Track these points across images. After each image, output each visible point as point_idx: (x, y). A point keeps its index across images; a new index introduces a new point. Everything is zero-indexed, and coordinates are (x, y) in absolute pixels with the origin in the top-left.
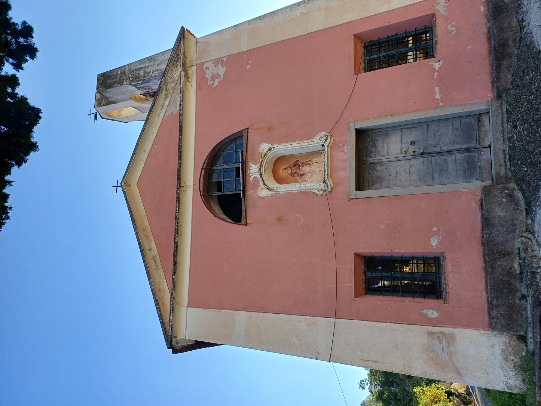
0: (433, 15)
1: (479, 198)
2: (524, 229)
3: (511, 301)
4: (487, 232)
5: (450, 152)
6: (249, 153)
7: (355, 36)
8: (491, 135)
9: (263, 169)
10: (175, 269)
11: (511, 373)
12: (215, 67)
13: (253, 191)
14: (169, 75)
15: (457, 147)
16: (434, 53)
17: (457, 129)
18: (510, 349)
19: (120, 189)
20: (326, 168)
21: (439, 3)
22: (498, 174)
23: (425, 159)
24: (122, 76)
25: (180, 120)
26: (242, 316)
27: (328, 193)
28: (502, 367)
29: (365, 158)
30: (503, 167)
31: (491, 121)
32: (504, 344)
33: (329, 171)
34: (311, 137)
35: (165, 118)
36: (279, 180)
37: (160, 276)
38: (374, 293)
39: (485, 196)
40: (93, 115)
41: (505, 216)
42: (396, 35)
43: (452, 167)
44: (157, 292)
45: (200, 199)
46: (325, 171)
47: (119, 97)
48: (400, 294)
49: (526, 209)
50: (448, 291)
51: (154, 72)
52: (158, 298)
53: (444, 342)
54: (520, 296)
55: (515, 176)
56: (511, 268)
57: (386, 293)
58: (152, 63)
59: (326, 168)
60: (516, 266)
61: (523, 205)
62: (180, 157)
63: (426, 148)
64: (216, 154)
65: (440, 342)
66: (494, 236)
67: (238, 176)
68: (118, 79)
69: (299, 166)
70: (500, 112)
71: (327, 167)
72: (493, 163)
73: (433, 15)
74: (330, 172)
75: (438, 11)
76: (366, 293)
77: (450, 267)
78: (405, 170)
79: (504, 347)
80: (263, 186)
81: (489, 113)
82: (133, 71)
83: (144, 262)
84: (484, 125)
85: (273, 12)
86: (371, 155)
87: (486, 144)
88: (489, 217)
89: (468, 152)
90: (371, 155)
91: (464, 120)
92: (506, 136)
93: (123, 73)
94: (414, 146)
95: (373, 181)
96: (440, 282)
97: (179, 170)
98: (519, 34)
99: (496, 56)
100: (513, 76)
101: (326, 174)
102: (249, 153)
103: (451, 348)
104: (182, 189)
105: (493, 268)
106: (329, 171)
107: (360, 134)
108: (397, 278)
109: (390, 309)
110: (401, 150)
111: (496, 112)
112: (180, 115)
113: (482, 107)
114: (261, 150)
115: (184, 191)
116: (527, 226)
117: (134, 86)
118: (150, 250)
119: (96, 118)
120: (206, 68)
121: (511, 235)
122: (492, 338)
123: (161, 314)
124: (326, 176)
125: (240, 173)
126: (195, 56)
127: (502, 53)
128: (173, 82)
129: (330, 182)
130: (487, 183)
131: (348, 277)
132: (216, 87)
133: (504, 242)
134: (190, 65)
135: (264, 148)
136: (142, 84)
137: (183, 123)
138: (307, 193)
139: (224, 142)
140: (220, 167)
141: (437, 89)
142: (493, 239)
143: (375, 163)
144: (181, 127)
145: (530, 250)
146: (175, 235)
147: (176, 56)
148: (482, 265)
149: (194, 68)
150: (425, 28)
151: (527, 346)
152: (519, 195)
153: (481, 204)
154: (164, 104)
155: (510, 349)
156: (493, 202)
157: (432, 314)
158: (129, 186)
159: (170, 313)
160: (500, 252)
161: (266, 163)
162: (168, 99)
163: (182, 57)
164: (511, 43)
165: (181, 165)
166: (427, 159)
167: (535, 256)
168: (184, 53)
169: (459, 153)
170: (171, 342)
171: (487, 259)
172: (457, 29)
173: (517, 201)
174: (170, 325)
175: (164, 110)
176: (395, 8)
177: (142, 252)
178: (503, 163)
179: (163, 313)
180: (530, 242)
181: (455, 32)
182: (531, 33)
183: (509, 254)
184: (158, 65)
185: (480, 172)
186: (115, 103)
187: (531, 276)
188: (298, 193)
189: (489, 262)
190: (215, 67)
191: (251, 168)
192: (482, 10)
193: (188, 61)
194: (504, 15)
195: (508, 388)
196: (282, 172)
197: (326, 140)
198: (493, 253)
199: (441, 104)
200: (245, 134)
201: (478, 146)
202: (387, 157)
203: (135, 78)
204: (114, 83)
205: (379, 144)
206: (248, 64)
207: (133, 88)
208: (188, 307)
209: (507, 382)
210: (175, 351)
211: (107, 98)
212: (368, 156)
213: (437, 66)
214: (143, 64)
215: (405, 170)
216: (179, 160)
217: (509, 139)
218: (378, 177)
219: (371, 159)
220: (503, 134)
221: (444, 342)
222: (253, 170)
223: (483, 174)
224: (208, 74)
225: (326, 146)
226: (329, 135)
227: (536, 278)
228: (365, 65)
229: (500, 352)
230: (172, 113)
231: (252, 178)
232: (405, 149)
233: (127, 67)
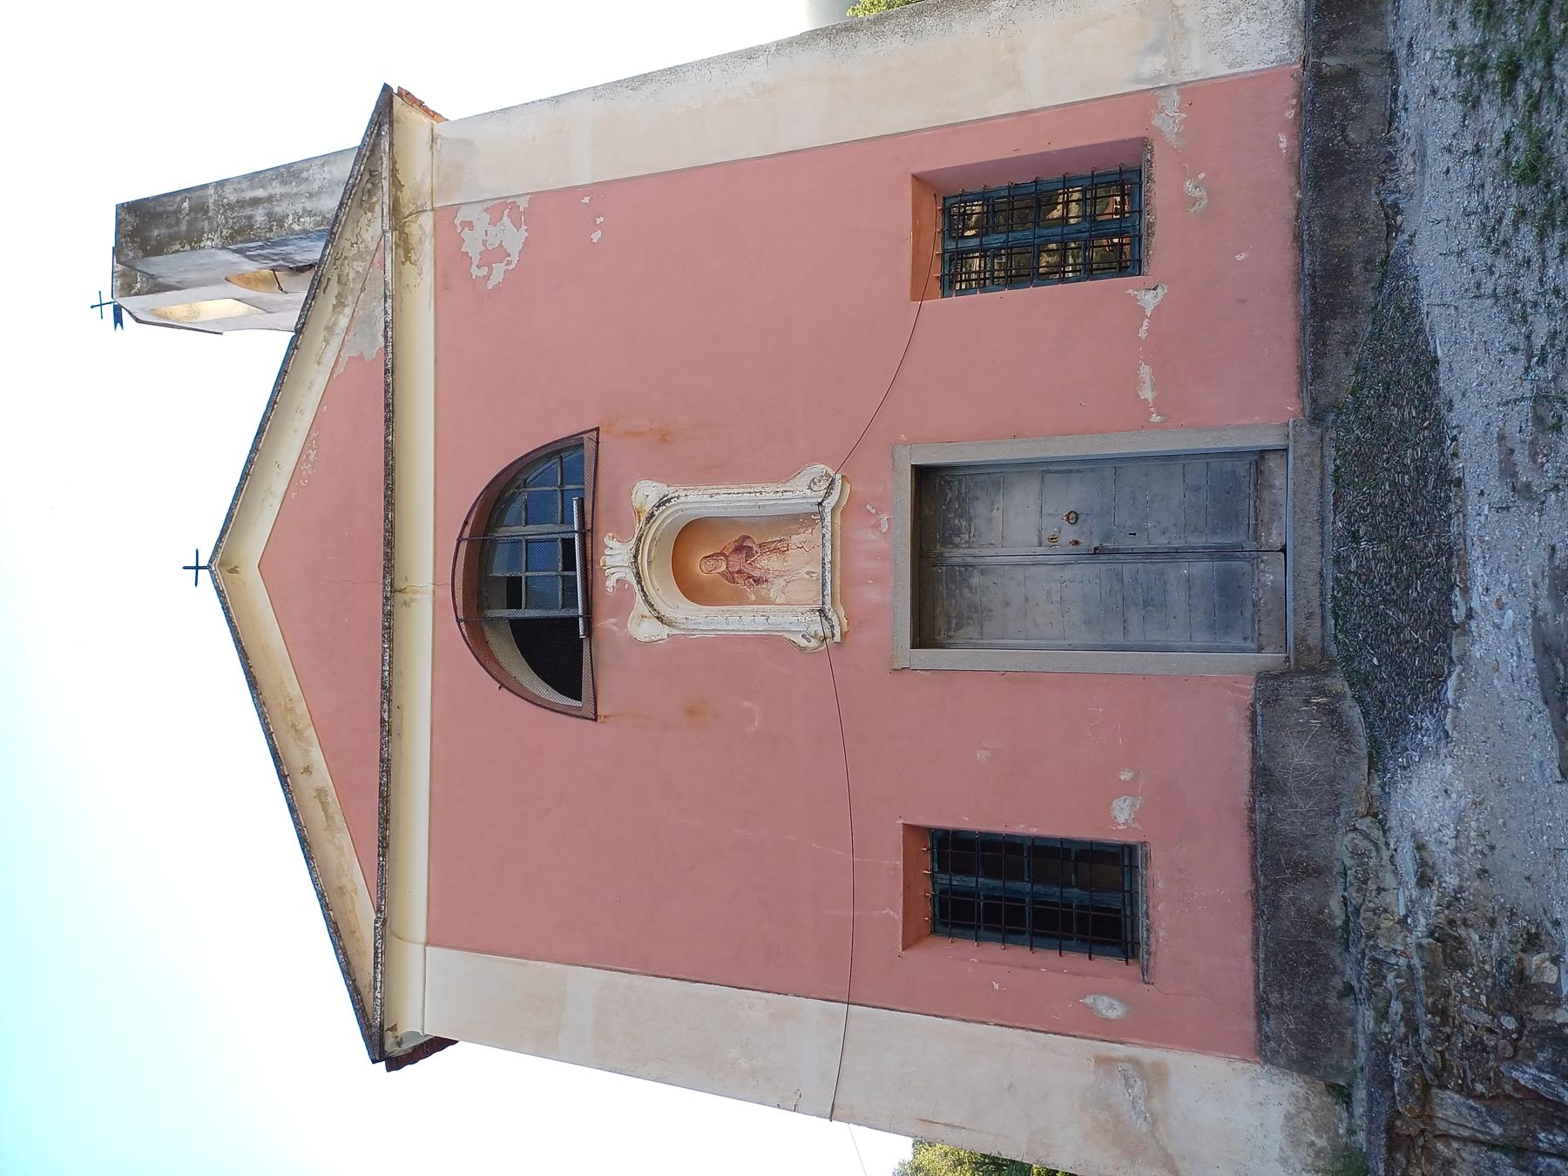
0: (1144, 143)
1: (1249, 699)
2: (1362, 808)
3: (1316, 999)
5: (1173, 554)
6: (601, 504)
7: (917, 178)
8: (1290, 515)
12: (493, 223)
13: (613, 620)
14: (348, 234)
15: (1195, 540)
17: (1197, 489)
18: (1308, 1115)
19: (204, 575)
22: (1301, 639)
23: (1104, 567)
24: (196, 220)
25: (387, 385)
26: (586, 982)
27: (834, 647)
28: (1284, 1161)
30: (1317, 622)
32: (1292, 1100)
33: (838, 582)
34: (784, 474)
35: (340, 370)
36: (692, 590)
37: (340, 849)
39: (1263, 706)
40: (109, 310)
41: (1314, 768)
42: (1036, 182)
43: (1177, 596)
44: (332, 899)
46: (824, 585)
47: (192, 276)
49: (1370, 755)
50: (1153, 949)
52: (339, 919)
54: (1340, 986)
55: (1349, 659)
56: (1321, 912)
58: (293, 188)
60: (1335, 904)
61: (1362, 745)
62: (390, 502)
63: (1107, 536)
64: (503, 492)
65: (1128, 1086)
66: (1280, 820)
67: (569, 564)
69: (749, 552)
70: (1317, 460)
72: (1290, 605)
73: (1144, 143)
74: (840, 583)
75: (1159, 132)
76: (934, 932)
77: (1160, 885)
78: (1049, 594)
79: (1292, 1110)
80: (645, 610)
82: (231, 207)
83: (292, 809)
84: (1272, 486)
86: (957, 540)
87: (1275, 540)
88: (1271, 765)
89: (1224, 558)
90: (957, 540)
92: (1331, 549)
93: (200, 209)
96: (1134, 916)
97: (389, 543)
98: (1383, 246)
99: (1314, 302)
100: (1357, 370)
101: (828, 591)
102: (602, 504)
103: (1156, 1103)
104: (400, 597)
105: (1275, 905)
106: (838, 582)
107: (924, 476)
108: (1019, 896)
110: (1040, 536)
111: (1307, 460)
112: (386, 371)
113: (1271, 440)
115: (405, 603)
116: (1370, 799)
117: (235, 251)
118: (307, 770)
119: (118, 319)
120: (463, 224)
121: (1326, 822)
122: (1262, 1082)
123: (348, 963)
124: (828, 599)
125: (576, 555)
127: (1332, 296)
128: (359, 256)
129: (838, 616)
130: (1271, 658)
131: (885, 886)
132: (497, 287)
133: (1307, 837)
134: (412, 207)
135: (645, 495)
136: (261, 247)
138: (773, 643)
141: (1145, 371)
142: (1278, 827)
143: (966, 566)
144: (390, 407)
145: (1372, 886)
146: (382, 738)
147: (366, 177)
148: (1246, 885)
149: (426, 221)
151: (1351, 1115)
152: (1356, 713)
153: (1253, 720)
154: (335, 324)
156: (1284, 727)
157: (1110, 1008)
158: (234, 570)
159: (376, 963)
160: (1296, 865)
162: (348, 311)
163: (386, 184)
164: (1357, 268)
166: (1112, 567)
167: (1385, 911)
168: (394, 171)
169: (1199, 559)
170: (382, 1045)
172: (1210, 195)
173: (1348, 730)
174: (375, 998)
175: (335, 342)
176: (1036, 107)
177: (283, 778)
178: (1318, 611)
179: (355, 961)
180: (1374, 854)
181: (1204, 203)
182: (1416, 279)
183: (1318, 872)
184: (311, 196)
187: (1372, 971)
188: (744, 637)
189: (1265, 888)
190: (493, 223)
191: (608, 552)
193: (406, 195)
194: (1345, 180)
196: (703, 568)
197: (828, 493)
198: (1279, 865)
199: (1155, 418)
200: (589, 446)
202: (1001, 551)
203: (240, 231)
204: (173, 238)
205: (979, 509)
206: (596, 227)
207: (236, 258)
208: (427, 944)
210: (394, 1064)
211: (151, 276)
212: (947, 541)
213: (1149, 300)
214: (263, 187)
215: (1049, 594)
216: (386, 509)
217: (1337, 560)
219: (957, 552)
220: (1322, 525)
222: (615, 558)
223: (1263, 625)
224: (473, 247)
225: (828, 510)
226: (838, 476)
227: (1385, 978)
229: (1281, 1121)
230: (361, 356)
231: (611, 583)
232: (1050, 533)
233: (211, 191)
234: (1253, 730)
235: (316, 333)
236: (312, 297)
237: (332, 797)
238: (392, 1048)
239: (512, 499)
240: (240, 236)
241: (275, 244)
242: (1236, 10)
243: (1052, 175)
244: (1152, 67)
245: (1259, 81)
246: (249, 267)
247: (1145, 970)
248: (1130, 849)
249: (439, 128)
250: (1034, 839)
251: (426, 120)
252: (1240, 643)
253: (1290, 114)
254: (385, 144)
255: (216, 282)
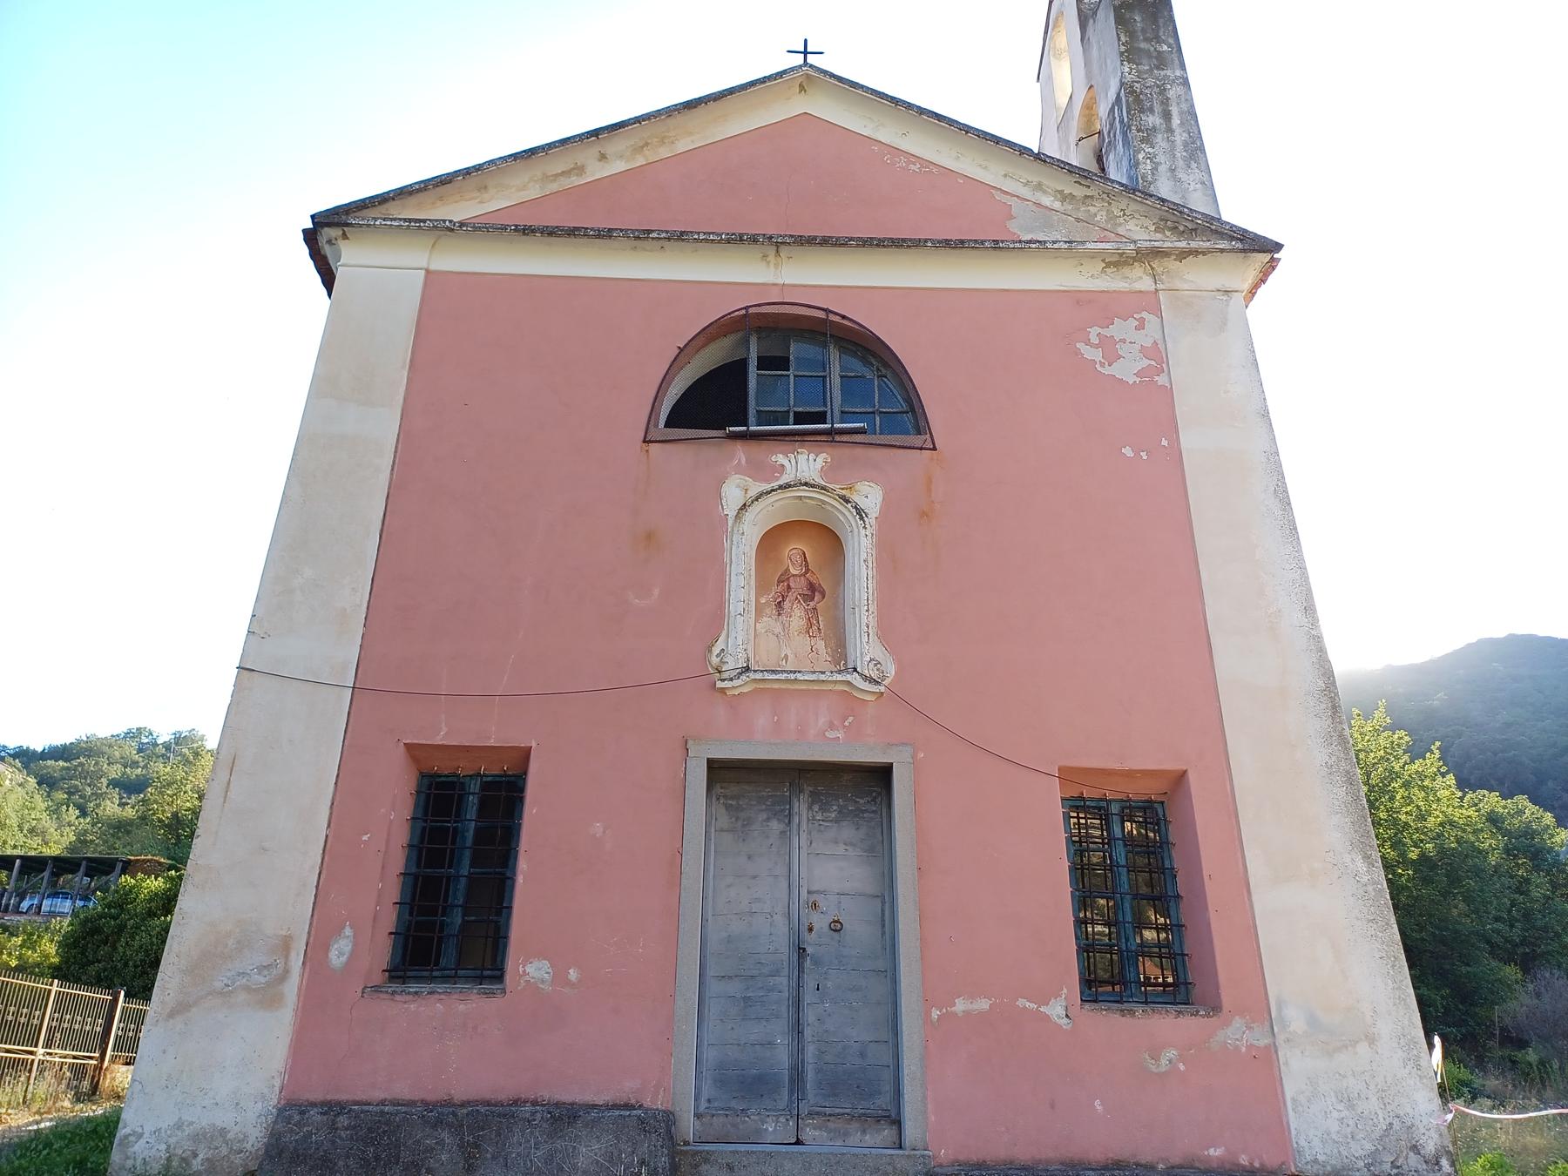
0: (1215, 1008)
1: (647, 1103)
3: (341, 1163)
4: (539, 1116)
5: (797, 1029)
6: (859, 451)
8: (832, 1149)
9: (804, 492)
10: (533, 231)
11: (163, 1147)
12: (1143, 349)
13: (743, 461)
14: (1133, 206)
15: (810, 1051)
16: (1103, 1006)
17: (862, 1055)
18: (225, 1151)
20: (782, 676)
21: (1249, 1028)
23: (785, 958)
24: (1150, 56)
25: (982, 242)
26: (384, 426)
27: (710, 681)
28: (179, 1126)
29: (808, 789)
31: (866, 1151)
33: (776, 686)
34: (886, 634)
36: (772, 540)
37: (524, 188)
38: (423, 796)
39: (639, 1117)
41: (575, 1167)
42: (1178, 897)
44: (474, 179)
45: (733, 305)
47: (1095, 52)
48: (414, 870)
50: (398, 997)
51: (1151, 157)
53: (263, 980)
57: (418, 832)
58: (1180, 153)
59: (782, 676)
62: (866, 243)
63: (817, 962)
64: (874, 355)
65: (261, 969)
66: (523, 1131)
67: (800, 418)
68: (1143, 45)
71: (787, 681)
72: (743, 1148)
73: (1215, 1008)
74: (776, 688)
75: (1228, 1024)
76: (423, 776)
77: (462, 1007)
78: (758, 900)
79: (230, 1136)
80: (753, 492)
81: (901, 1148)
82: (1163, 91)
84: (864, 1132)
85: (1294, 529)
86: (816, 807)
87: (809, 1134)
89: (791, 1080)
90: (816, 807)
91: (887, 1075)
93: (1161, 62)
94: (826, 929)
95: (739, 809)
97: (825, 242)
102: (860, 451)
103: (242, 997)
104: (771, 251)
105: (438, 1123)
106: (776, 686)
107: (881, 775)
109: (365, 838)
110: (817, 892)
112: (996, 242)
113: (911, 1132)
114: (864, 487)
115: (765, 256)
118: (603, 157)
120: (1142, 321)
124: (759, 676)
125: (809, 425)
126: (1186, 286)
128: (1111, 218)
129: (741, 685)
130: (688, 1126)
131: (468, 728)
132: (1078, 352)
134: (1159, 270)
135: (865, 493)
136: (1122, 121)
137: (974, 252)
138: (717, 620)
139: (904, 377)
140: (836, 364)
141: (983, 1004)
144: (960, 244)
146: (633, 231)
147: (1190, 226)
149: (1146, 284)
150: (1187, 984)
153: (628, 1106)
154: (1045, 192)
155: (225, 1151)
157: (339, 952)
158: (802, 88)
159: (410, 220)
160: (477, 1146)
161: (824, 502)
162: (1057, 205)
163: (1183, 244)
165: (841, 245)
168: (1196, 252)
169: (791, 1055)
170: (329, 225)
171: (465, 1111)
172: (1160, 1075)
174: (375, 219)
177: (596, 133)
179: (413, 200)
181: (1154, 1069)
184: (1173, 171)
185: (729, 1109)
186: (1082, 40)
192: (1212, 1151)
193: (1172, 264)
195: (126, 1137)
196: (793, 551)
197: (865, 678)
199: (935, 1014)
201: (804, 1110)
203: (1138, 100)
204: (1132, 34)
205: (848, 831)
206: (1137, 453)
208: (428, 271)
209: (141, 1136)
210: (310, 237)
212: (815, 796)
213: (1055, 1010)
214: (1182, 124)
215: (758, 900)
218: (748, 822)
221: (263, 980)
222: (806, 463)
223: (722, 1119)
224: (1119, 329)
225: (849, 678)
226: (882, 689)
228: (1092, 800)
229: (219, 1124)
230: (1011, 217)
231: (780, 459)
232: (822, 905)
233: (1178, 73)
234: (615, 1106)
235: (1035, 174)
236: (1071, 170)
237: (576, 181)
238: (326, 234)
239: (867, 363)
240: (1133, 100)
241: (1125, 134)
242: (1351, 1107)
243: (1185, 913)
244: (1293, 1018)
245: (1282, 1127)
246: (1103, 109)
247: (376, 989)
248: (499, 977)
249: (1238, 299)
250: (513, 880)
251: (1246, 286)
252: (705, 1096)
253: (1244, 1160)
254: (1223, 245)
255: (1089, 75)
